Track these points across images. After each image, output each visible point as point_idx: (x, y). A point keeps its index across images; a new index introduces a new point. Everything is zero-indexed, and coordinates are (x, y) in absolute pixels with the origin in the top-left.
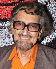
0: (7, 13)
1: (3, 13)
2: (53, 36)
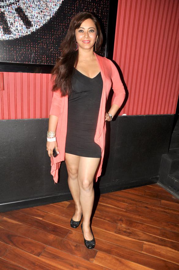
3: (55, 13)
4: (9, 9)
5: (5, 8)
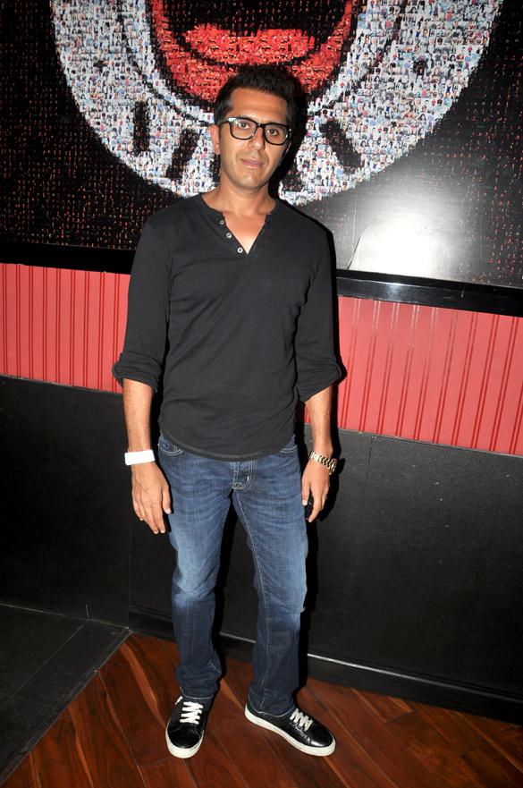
1: (276, 41)
2: (389, 156)
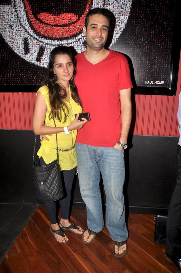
0: (70, 17)
1: (59, 33)
3: (117, 40)
4: (77, 43)
5: (75, 43)
